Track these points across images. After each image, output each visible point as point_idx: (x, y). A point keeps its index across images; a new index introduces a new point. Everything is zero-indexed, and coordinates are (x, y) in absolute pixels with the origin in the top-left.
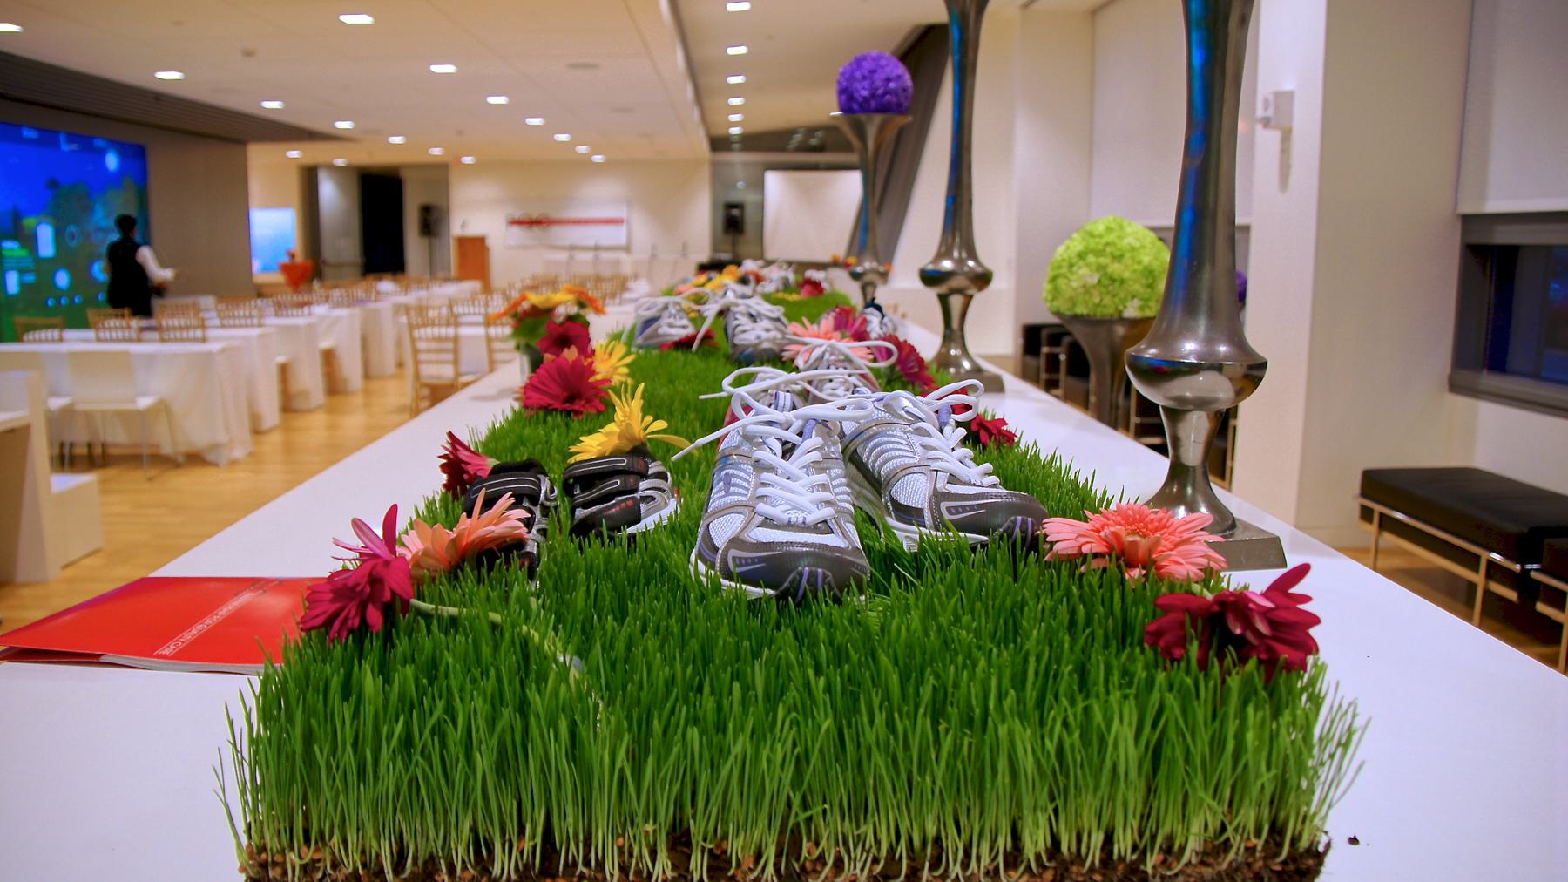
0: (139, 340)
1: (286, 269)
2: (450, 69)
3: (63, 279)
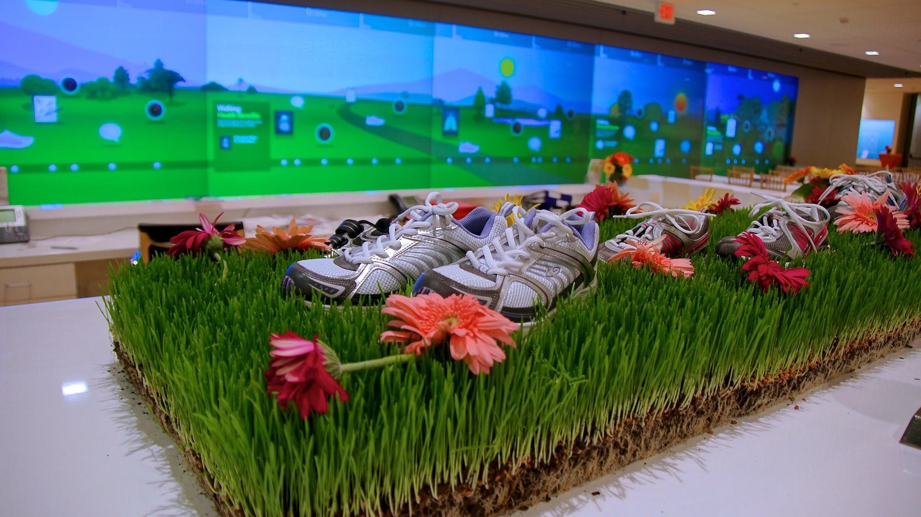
0: (750, 186)
1: (881, 157)
2: (875, 53)
3: (737, 150)
